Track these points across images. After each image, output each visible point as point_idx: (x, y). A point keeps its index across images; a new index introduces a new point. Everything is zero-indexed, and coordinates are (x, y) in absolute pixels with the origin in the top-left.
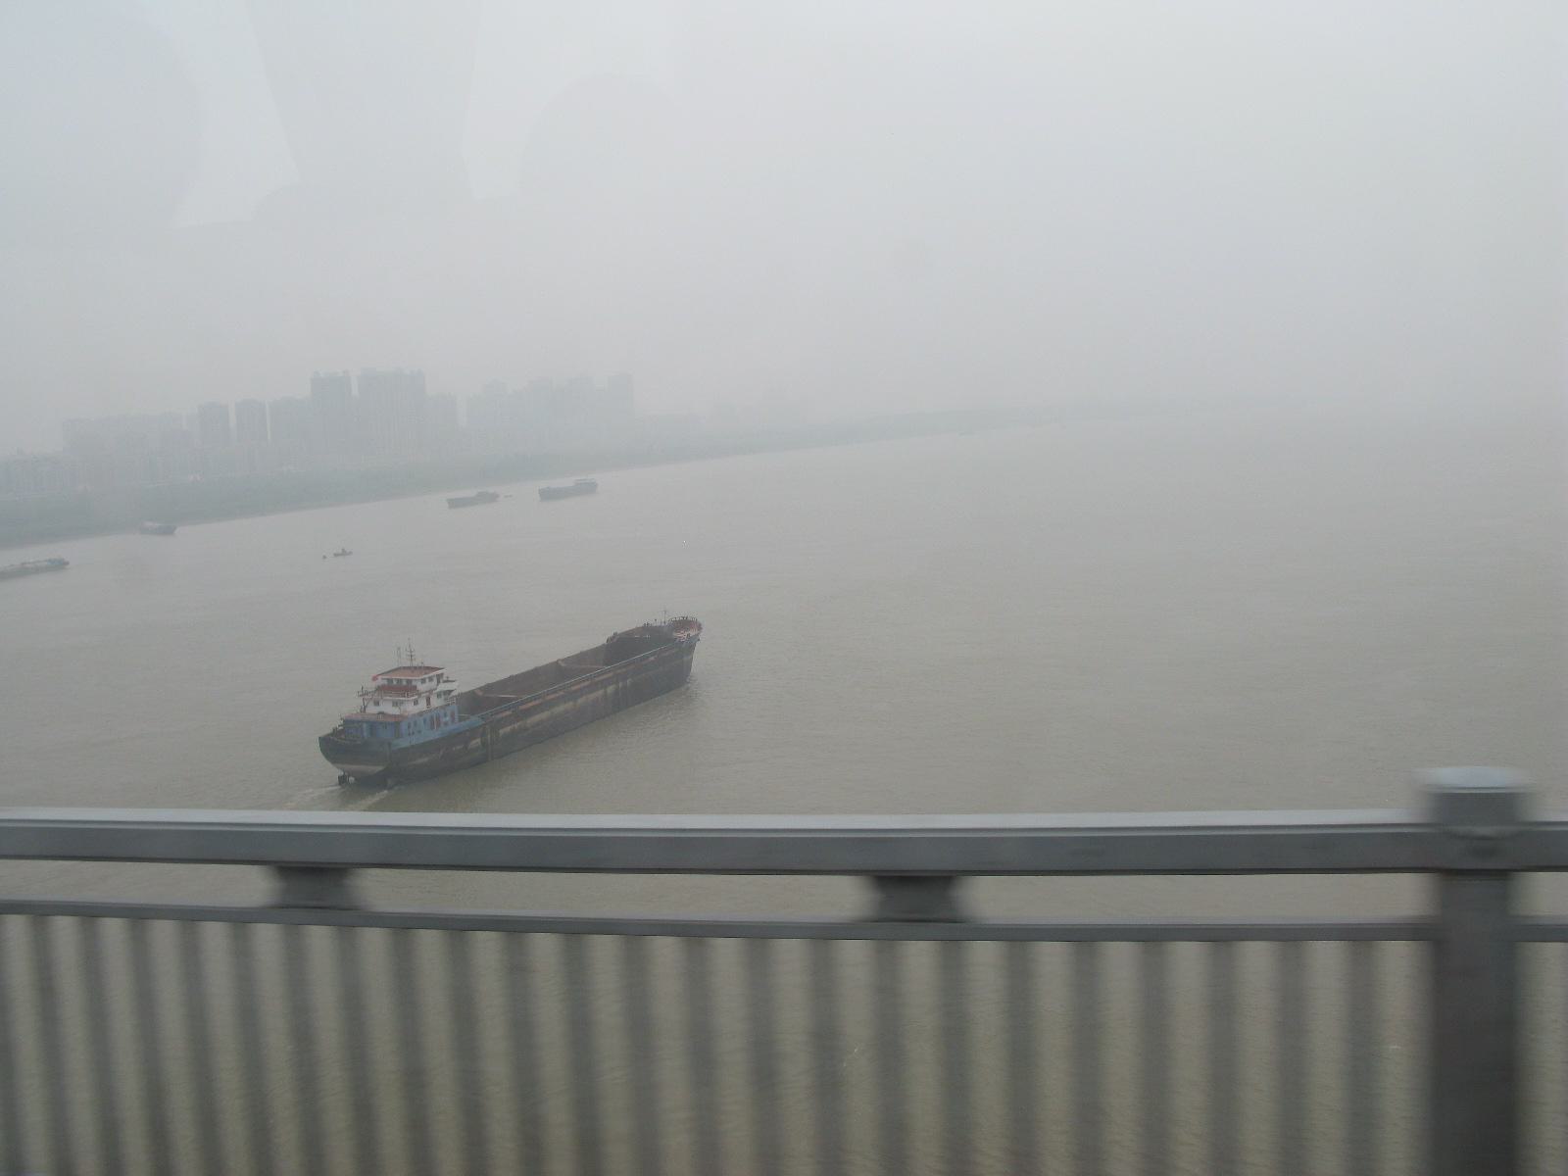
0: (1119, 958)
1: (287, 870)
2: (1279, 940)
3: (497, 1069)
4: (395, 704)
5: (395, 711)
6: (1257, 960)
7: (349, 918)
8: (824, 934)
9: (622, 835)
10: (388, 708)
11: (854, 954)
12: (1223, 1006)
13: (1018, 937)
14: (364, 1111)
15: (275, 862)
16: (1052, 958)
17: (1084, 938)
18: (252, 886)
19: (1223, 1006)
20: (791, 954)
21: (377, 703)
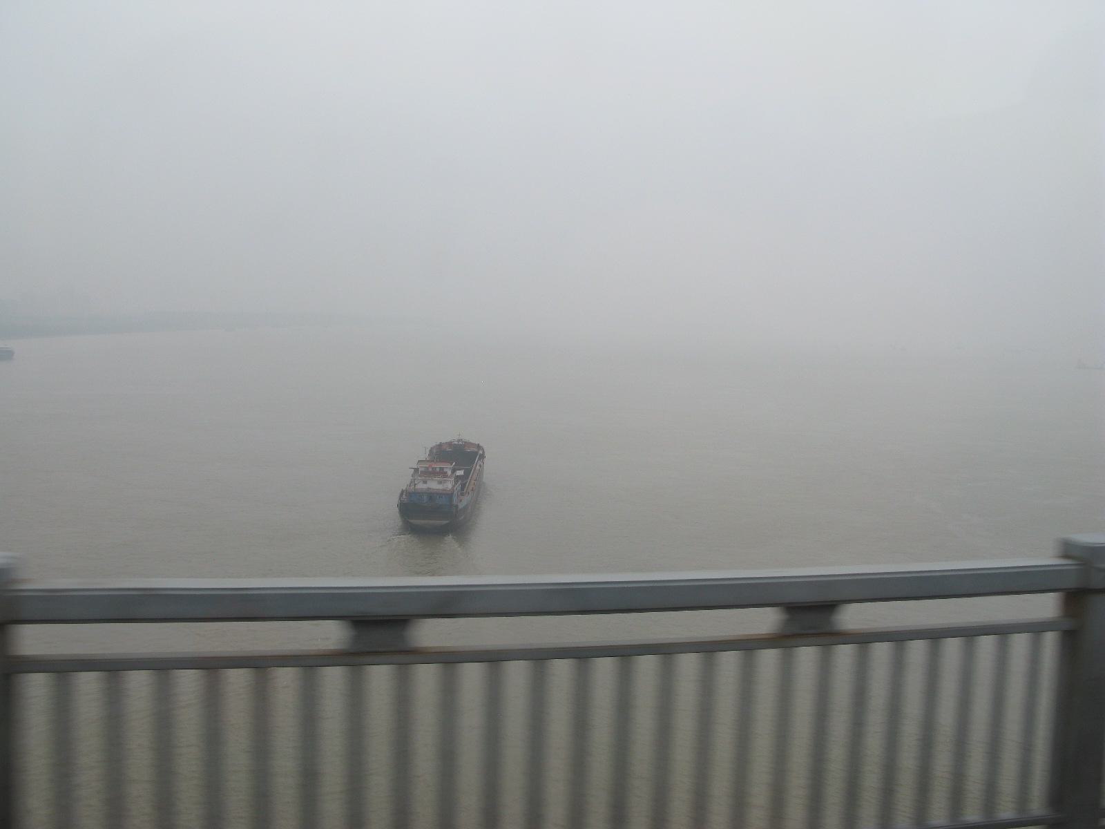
0: (688, 664)
1: (793, 609)
2: (532, 660)
3: (874, 744)
4: (440, 483)
5: (440, 487)
6: (188, 683)
7: (830, 637)
8: (309, 663)
9: (299, 592)
10: (434, 485)
11: (333, 678)
12: (164, 723)
13: (450, 659)
14: (309, 777)
15: (1065, 589)
16: (237, 681)
17: (211, 666)
18: (765, 620)
19: (164, 723)
20: (286, 680)
21: (425, 482)
